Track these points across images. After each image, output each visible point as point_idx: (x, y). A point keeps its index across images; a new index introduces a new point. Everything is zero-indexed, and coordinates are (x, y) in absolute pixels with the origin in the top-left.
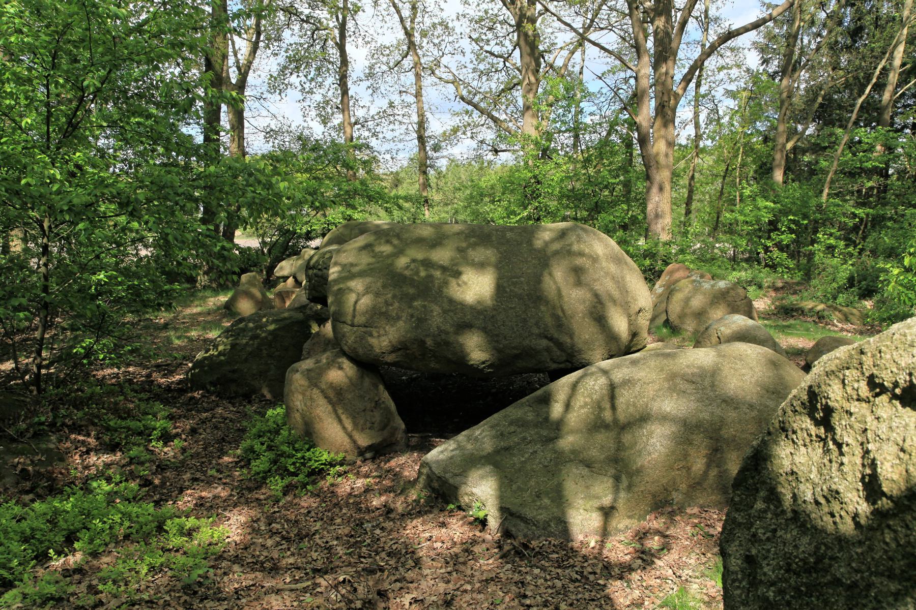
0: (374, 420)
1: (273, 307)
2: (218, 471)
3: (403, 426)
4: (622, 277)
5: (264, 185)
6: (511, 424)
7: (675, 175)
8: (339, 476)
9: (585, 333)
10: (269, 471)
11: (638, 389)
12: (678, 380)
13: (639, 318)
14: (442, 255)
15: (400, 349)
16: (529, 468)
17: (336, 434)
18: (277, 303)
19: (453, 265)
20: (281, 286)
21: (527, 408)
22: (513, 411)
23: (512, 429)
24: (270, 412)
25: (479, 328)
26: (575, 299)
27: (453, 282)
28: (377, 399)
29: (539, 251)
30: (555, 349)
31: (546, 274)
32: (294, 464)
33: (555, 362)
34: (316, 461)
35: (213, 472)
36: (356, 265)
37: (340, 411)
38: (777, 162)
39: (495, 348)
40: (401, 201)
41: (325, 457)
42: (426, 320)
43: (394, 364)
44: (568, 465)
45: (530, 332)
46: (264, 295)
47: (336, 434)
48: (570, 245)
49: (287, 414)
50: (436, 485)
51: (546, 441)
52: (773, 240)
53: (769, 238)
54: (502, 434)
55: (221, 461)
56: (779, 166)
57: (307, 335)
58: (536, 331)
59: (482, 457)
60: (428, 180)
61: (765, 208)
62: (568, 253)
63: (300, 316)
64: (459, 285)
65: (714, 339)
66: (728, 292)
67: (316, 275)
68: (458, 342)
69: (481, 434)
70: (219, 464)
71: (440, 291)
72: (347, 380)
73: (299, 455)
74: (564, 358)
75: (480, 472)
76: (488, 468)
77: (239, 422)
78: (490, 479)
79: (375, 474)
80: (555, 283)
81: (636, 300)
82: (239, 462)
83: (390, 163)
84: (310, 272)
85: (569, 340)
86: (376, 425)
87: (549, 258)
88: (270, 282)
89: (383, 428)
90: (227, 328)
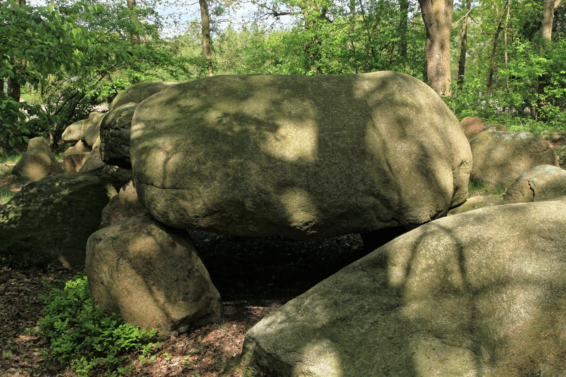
0: (187, 290)
1: (62, 171)
2: (14, 352)
3: (218, 295)
4: (445, 128)
5: (54, 33)
6: (345, 290)
7: (454, 33)
8: (152, 354)
9: (411, 187)
10: (73, 351)
11: (490, 248)
12: (535, 238)
13: (461, 171)
14: (255, 107)
15: (215, 212)
16: (371, 340)
17: (145, 308)
18: (68, 167)
19: (269, 119)
20: (70, 150)
21: (360, 273)
22: (345, 277)
23: (347, 296)
24: (69, 284)
25: (301, 187)
26: (401, 154)
27: (271, 137)
28: (190, 267)
29: (360, 101)
30: (381, 207)
31: (369, 125)
32: (101, 342)
33: (381, 221)
34: (126, 339)
35: (9, 354)
36: (161, 121)
38: (546, 20)
39: (319, 208)
40: (187, 64)
41: (136, 334)
42: (244, 179)
43: (209, 229)
44: (415, 336)
45: (355, 188)
46: (53, 159)
47: (145, 308)
48: (393, 94)
49: (90, 286)
50: (265, 362)
51: (387, 309)
52: (546, 94)
53: (541, 92)
54: (336, 303)
55: (17, 340)
56: (548, 23)
57: (105, 200)
58: (362, 188)
59: (315, 330)
60: (211, 43)
61: (538, 63)
62: (390, 103)
63: (95, 179)
64: (277, 140)
65: (527, 192)
66: (530, 143)
67: (112, 135)
68: (279, 202)
69: (310, 304)
70: (15, 344)
71: (257, 148)
72: (158, 248)
73: (106, 333)
74: (390, 217)
75: (317, 348)
76: (325, 343)
77: (35, 294)
78: (328, 355)
79: (193, 350)
80: (380, 135)
81: (458, 152)
82: (38, 340)
83: (173, 27)
84: (106, 132)
85: (396, 197)
86: (190, 295)
87: (371, 110)
88: (58, 146)
89: (197, 299)
90: (17, 193)
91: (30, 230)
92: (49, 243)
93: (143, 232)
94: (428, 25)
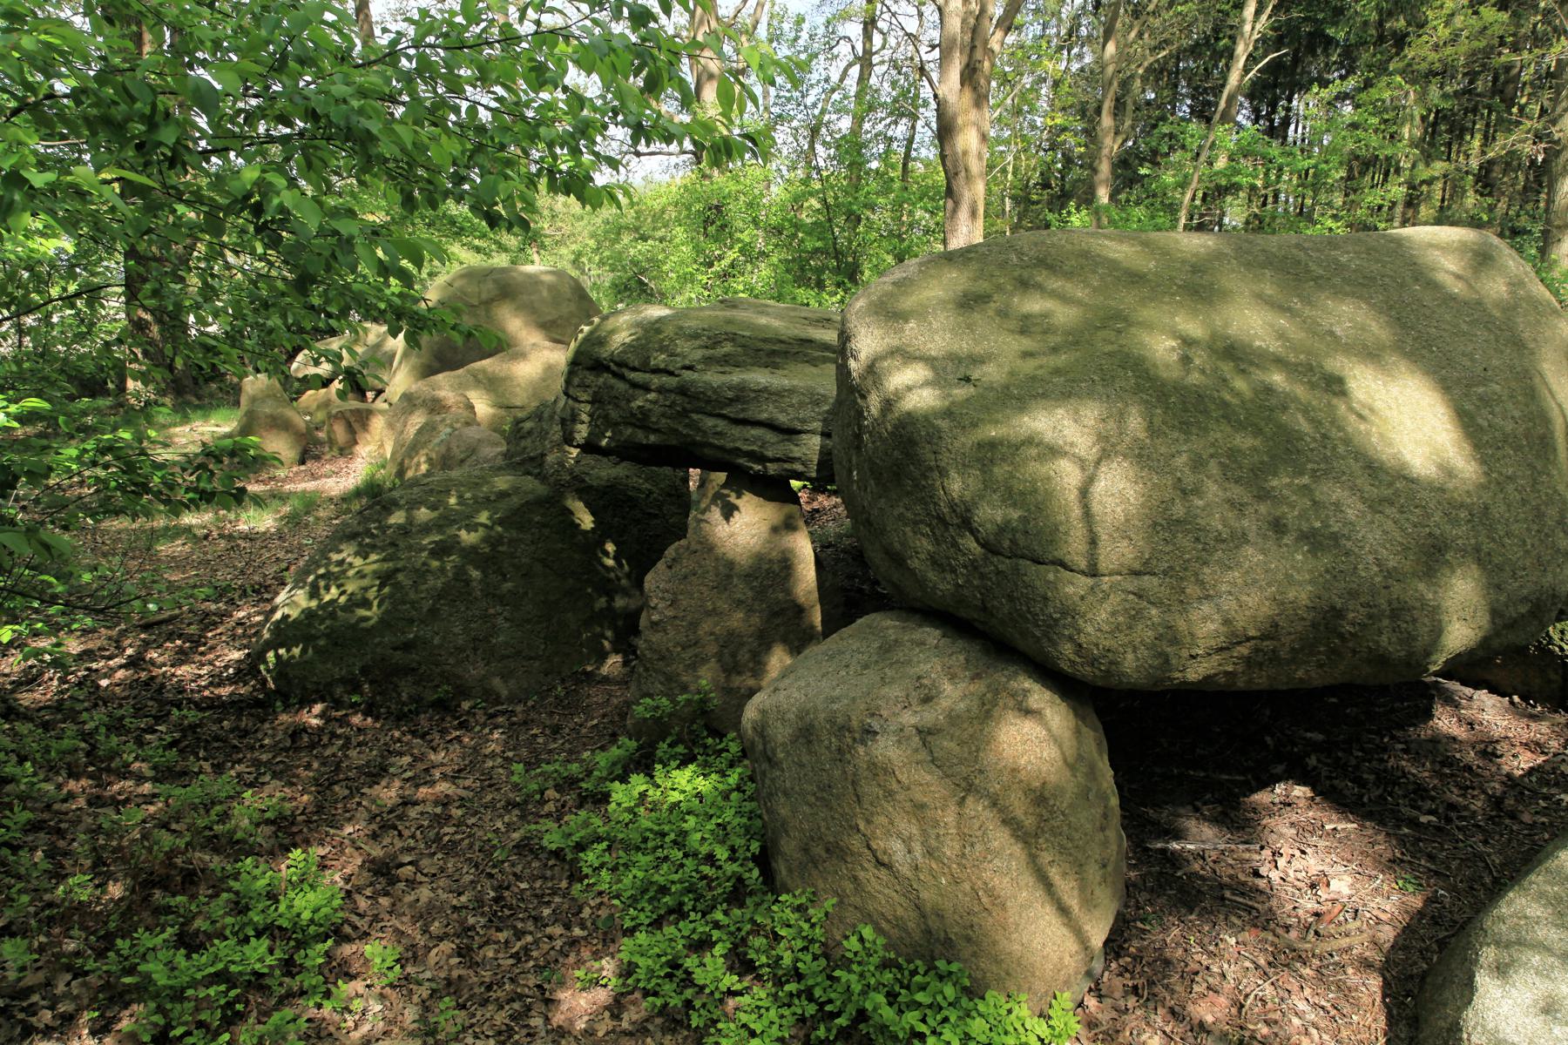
37: (1045, 857)
91: (411, 621)
92: (460, 650)
93: (1005, 707)
94: (951, 176)
